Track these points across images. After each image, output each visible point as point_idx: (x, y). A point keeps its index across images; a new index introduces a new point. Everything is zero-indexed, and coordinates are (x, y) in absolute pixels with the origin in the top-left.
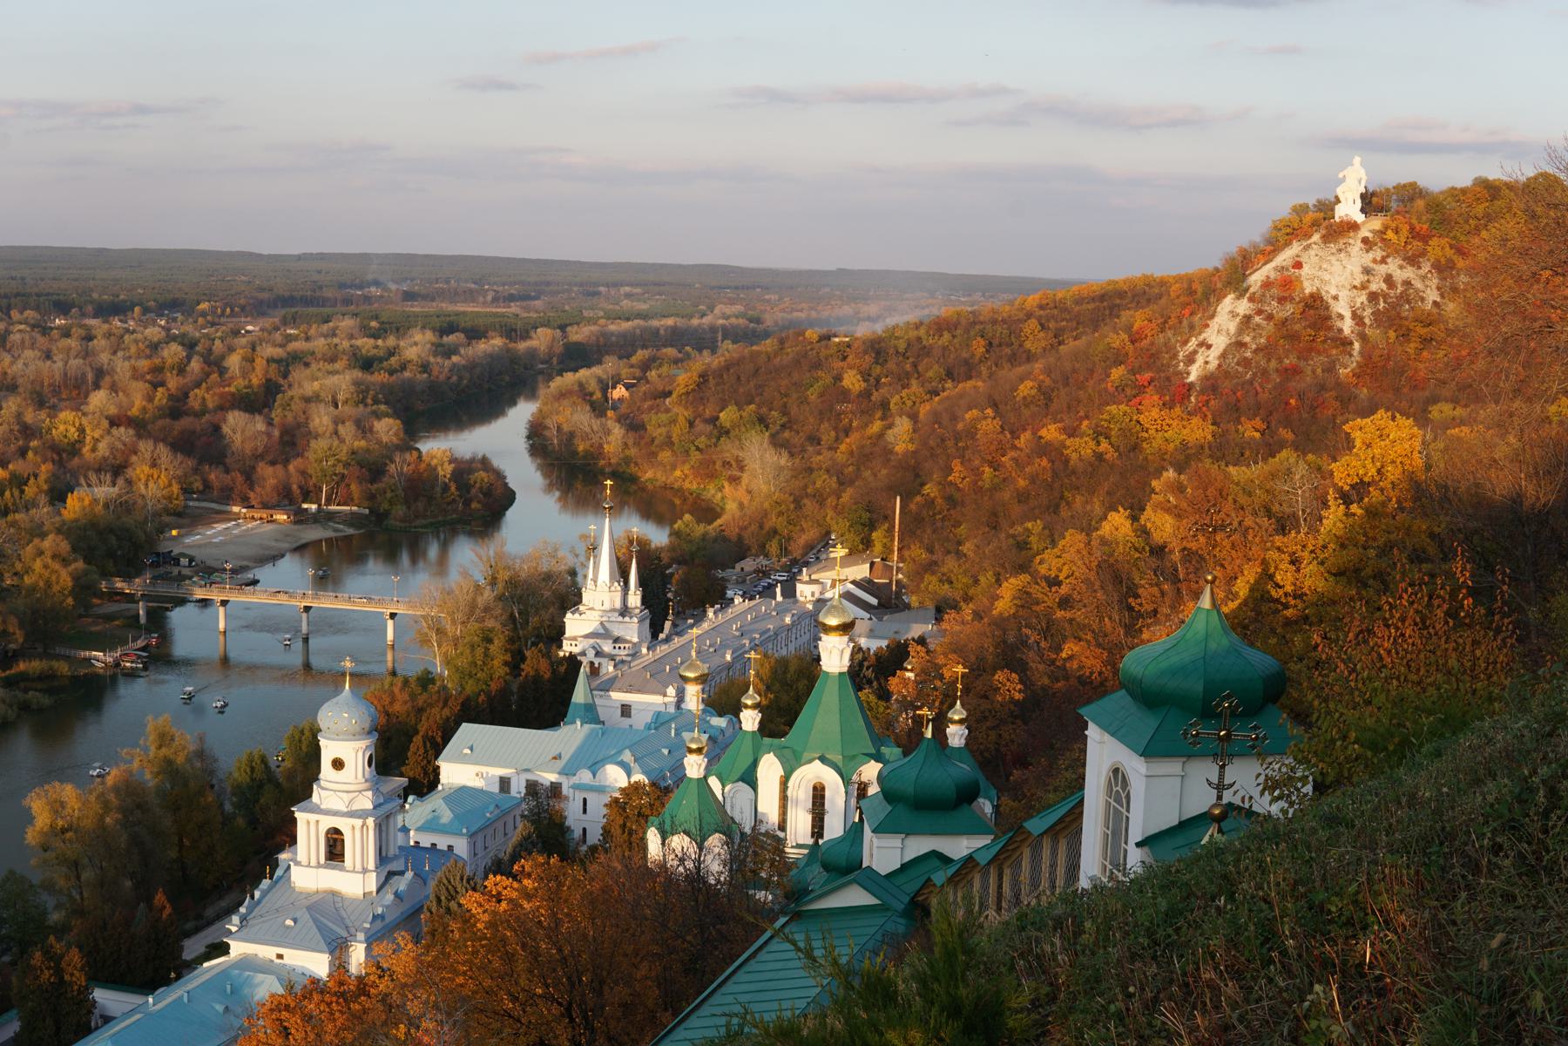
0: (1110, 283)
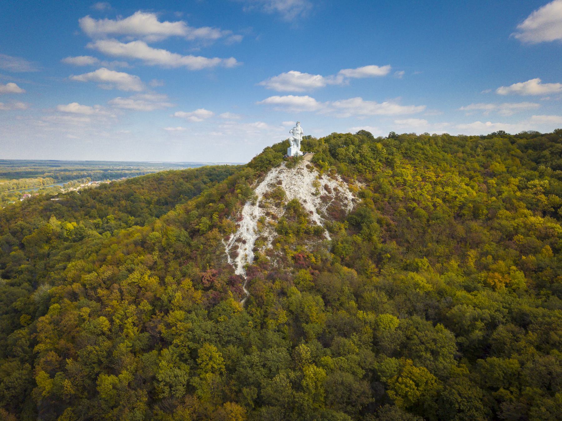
0: (217, 164)
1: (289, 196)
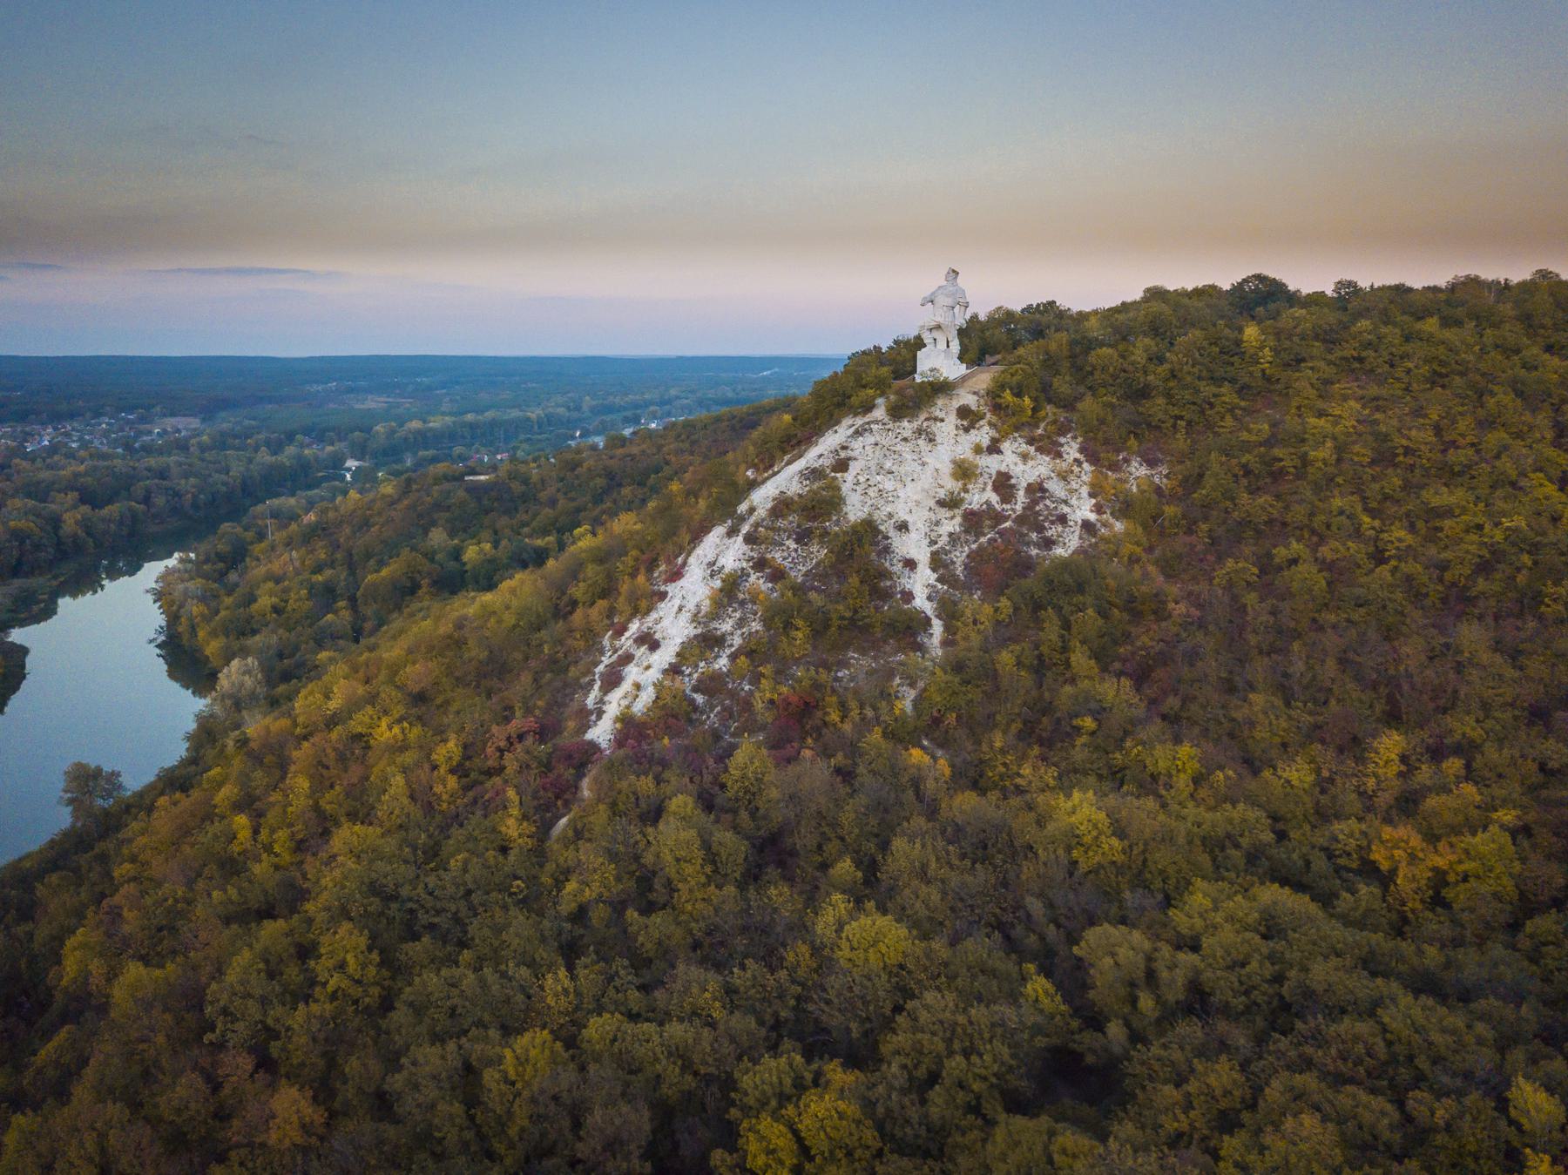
1: (855, 509)
